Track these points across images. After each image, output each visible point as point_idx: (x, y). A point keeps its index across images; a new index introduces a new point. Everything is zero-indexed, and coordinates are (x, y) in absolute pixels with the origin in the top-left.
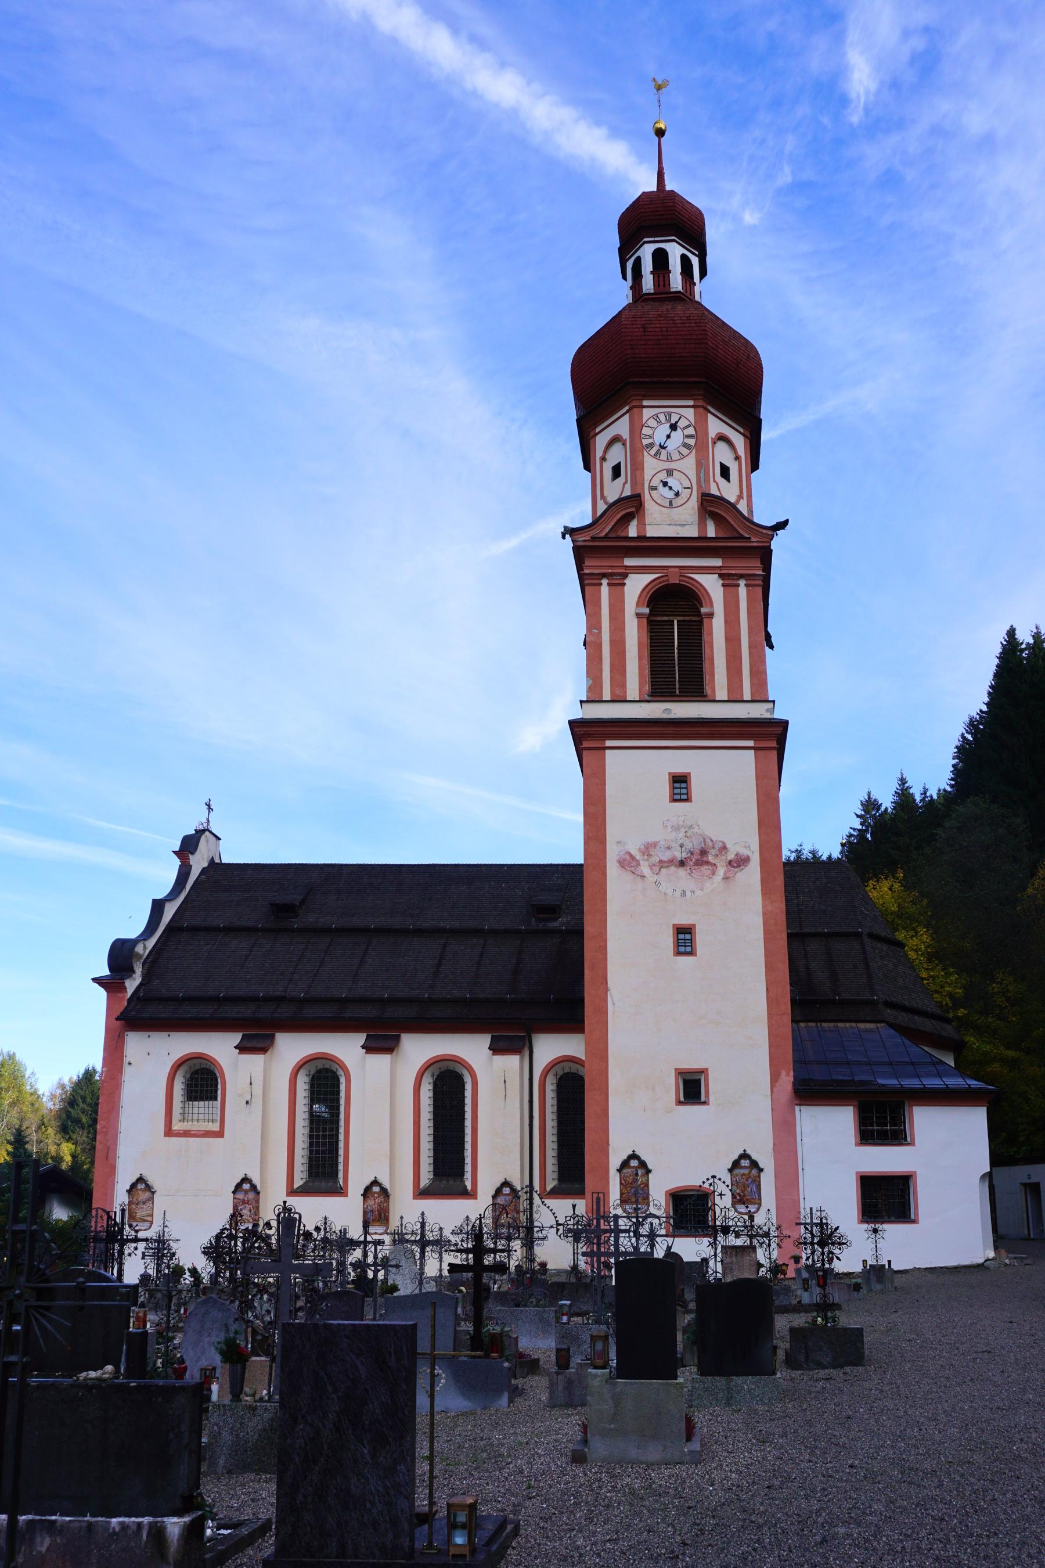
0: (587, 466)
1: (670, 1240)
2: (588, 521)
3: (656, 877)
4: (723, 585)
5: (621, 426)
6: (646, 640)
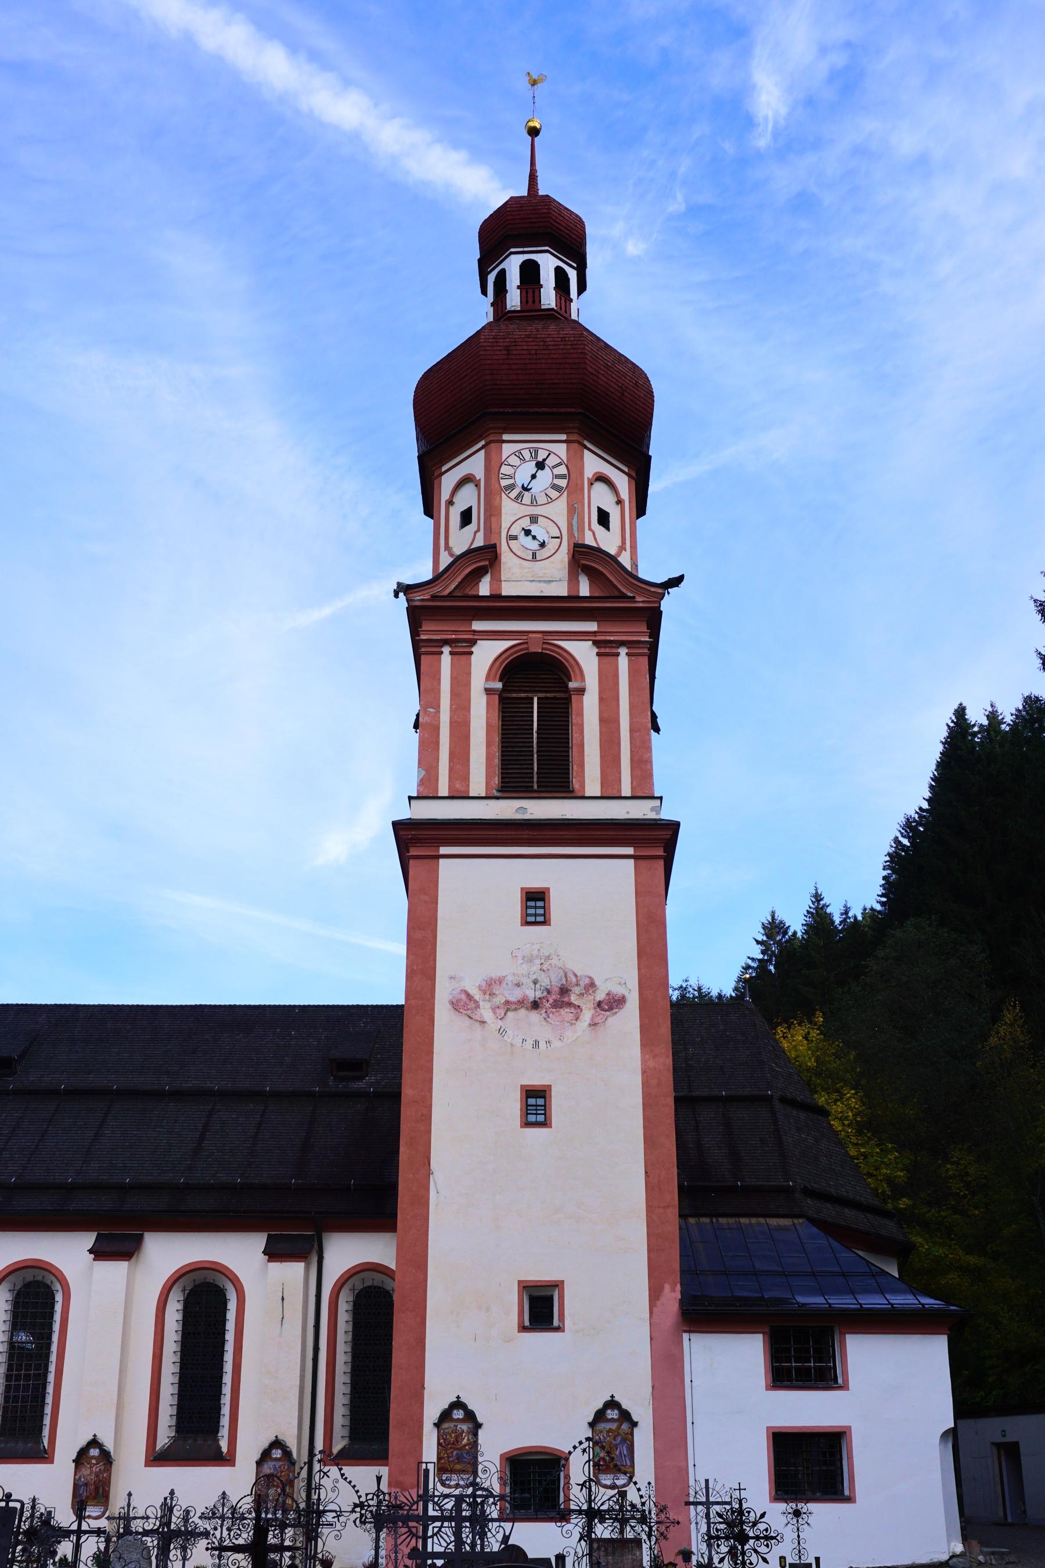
0: (429, 510)
1: (507, 1526)
2: (428, 576)
3: (500, 1023)
4: (598, 654)
5: (475, 464)
6: (496, 721)
